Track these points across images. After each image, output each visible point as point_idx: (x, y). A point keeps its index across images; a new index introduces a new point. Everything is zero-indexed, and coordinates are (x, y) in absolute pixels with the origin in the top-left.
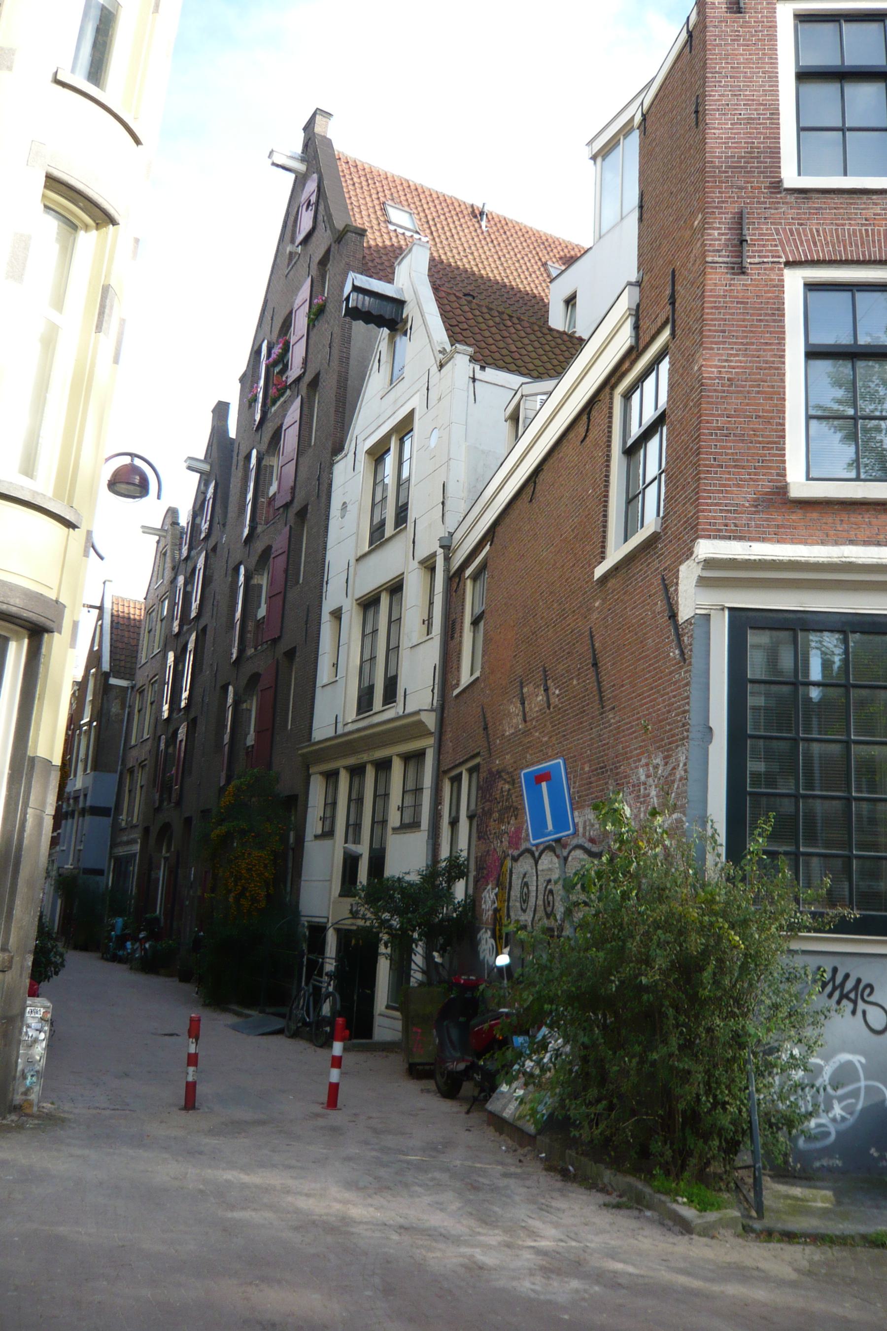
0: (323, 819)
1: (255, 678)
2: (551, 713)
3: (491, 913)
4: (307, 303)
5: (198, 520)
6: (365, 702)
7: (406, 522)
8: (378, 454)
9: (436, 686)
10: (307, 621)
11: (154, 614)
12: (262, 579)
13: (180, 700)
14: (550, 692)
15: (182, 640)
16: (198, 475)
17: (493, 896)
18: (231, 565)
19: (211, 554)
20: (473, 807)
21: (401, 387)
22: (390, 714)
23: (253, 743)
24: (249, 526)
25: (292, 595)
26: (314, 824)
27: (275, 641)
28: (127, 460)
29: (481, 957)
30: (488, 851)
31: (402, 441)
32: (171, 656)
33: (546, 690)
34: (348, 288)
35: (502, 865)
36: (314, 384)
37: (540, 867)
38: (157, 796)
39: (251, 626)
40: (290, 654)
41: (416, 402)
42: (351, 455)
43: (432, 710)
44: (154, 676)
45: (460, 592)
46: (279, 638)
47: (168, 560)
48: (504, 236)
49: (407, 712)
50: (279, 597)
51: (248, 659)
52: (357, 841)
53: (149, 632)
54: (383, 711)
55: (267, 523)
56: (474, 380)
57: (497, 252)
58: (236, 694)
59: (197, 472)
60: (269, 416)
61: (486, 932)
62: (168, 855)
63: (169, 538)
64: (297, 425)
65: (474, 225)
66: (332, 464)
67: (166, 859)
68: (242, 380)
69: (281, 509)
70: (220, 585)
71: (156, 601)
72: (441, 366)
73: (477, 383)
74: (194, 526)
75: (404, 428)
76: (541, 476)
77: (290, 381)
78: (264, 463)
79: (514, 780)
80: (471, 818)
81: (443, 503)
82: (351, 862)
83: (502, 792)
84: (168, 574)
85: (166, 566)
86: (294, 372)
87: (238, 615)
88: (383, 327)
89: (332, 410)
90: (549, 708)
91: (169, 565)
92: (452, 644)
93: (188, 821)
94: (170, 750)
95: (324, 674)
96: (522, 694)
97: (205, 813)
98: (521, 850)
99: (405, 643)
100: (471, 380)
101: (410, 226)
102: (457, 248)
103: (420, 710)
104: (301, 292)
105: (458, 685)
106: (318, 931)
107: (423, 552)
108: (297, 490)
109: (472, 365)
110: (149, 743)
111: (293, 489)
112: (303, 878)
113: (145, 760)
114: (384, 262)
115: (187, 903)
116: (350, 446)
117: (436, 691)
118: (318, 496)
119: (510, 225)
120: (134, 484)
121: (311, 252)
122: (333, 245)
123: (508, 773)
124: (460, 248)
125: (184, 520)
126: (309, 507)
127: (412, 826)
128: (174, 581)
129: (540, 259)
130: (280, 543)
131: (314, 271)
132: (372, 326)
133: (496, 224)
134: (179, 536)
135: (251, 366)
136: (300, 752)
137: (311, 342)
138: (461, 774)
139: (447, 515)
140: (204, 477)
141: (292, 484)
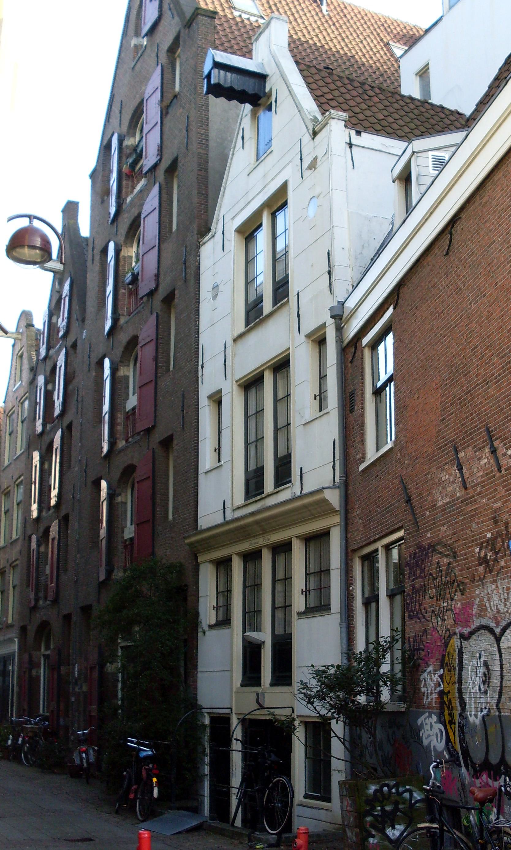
0: (216, 608)
1: (129, 470)
2: (503, 476)
3: (434, 696)
4: (159, 91)
5: (54, 319)
6: (254, 484)
7: (287, 296)
8: (248, 232)
9: (337, 463)
10: (183, 406)
11: (14, 416)
12: (129, 371)
13: (50, 499)
14: (499, 453)
15: (46, 439)
16: (52, 274)
17: (436, 678)
18: (94, 360)
19: (71, 352)
20: (392, 586)
21: (270, 161)
22: (285, 495)
23: (132, 535)
24: (112, 318)
25: (165, 383)
26: (208, 614)
27: (148, 431)
28: (24, 223)
29: (425, 742)
30: (425, 631)
31: (274, 216)
32: (36, 457)
33: (494, 451)
34: (208, 66)
35: (446, 645)
36: (172, 169)
37: (503, 645)
38: (32, 595)
39: (120, 417)
40: (167, 443)
41: (290, 174)
42: (219, 235)
43: (334, 487)
44: (19, 477)
45: (357, 362)
46: (153, 427)
47: (25, 361)
48: (344, 19)
49: (304, 492)
50: (151, 386)
51: (120, 452)
52: (257, 628)
53: (10, 434)
54: (277, 492)
55: (129, 314)
56: (351, 145)
57: (340, 34)
58: (109, 487)
59: (51, 271)
60: (124, 206)
61: (430, 716)
62: (48, 652)
63: (24, 340)
64: (157, 212)
65: (314, 9)
66: (198, 247)
67: (46, 657)
68: (93, 176)
69: (145, 299)
70: (83, 381)
71: (16, 403)
72: (315, 134)
73: (354, 148)
74: (51, 326)
75: (278, 202)
76: (459, 226)
77: (145, 169)
78: (122, 254)
79: (455, 553)
80: (391, 596)
81: (329, 273)
82: (252, 652)
83: (439, 566)
84: (26, 375)
85: (23, 368)
86: (148, 161)
87: (106, 407)
88: (246, 102)
89: (195, 192)
90: (499, 470)
91: (26, 367)
92: (352, 418)
93: (67, 618)
94: (42, 549)
95: (206, 458)
96: (458, 459)
97: (86, 610)
98: (473, 627)
99: (296, 421)
100: (348, 146)
101: (255, 12)
102: (301, 31)
103: (323, 488)
104: (150, 82)
105: (363, 459)
106: (221, 723)
107: (309, 325)
108: (162, 277)
109: (347, 131)
110: (20, 543)
111: (157, 276)
112: (200, 669)
113: (16, 560)
114: (244, 38)
115: (73, 699)
116: (217, 227)
117: (337, 467)
118: (186, 280)
119: (349, 8)
120: (35, 247)
121: (158, 41)
122: (183, 31)
123: (445, 546)
124: (305, 31)
125: (40, 321)
126: (176, 292)
127: (319, 607)
128: (33, 381)
129: (382, 40)
130: (147, 331)
131: (163, 58)
132: (234, 102)
133: (335, 8)
134: (34, 338)
135: (101, 162)
136: (187, 541)
137: (166, 129)
138: (377, 550)
139: (335, 284)
140: (58, 276)
141: (156, 271)
